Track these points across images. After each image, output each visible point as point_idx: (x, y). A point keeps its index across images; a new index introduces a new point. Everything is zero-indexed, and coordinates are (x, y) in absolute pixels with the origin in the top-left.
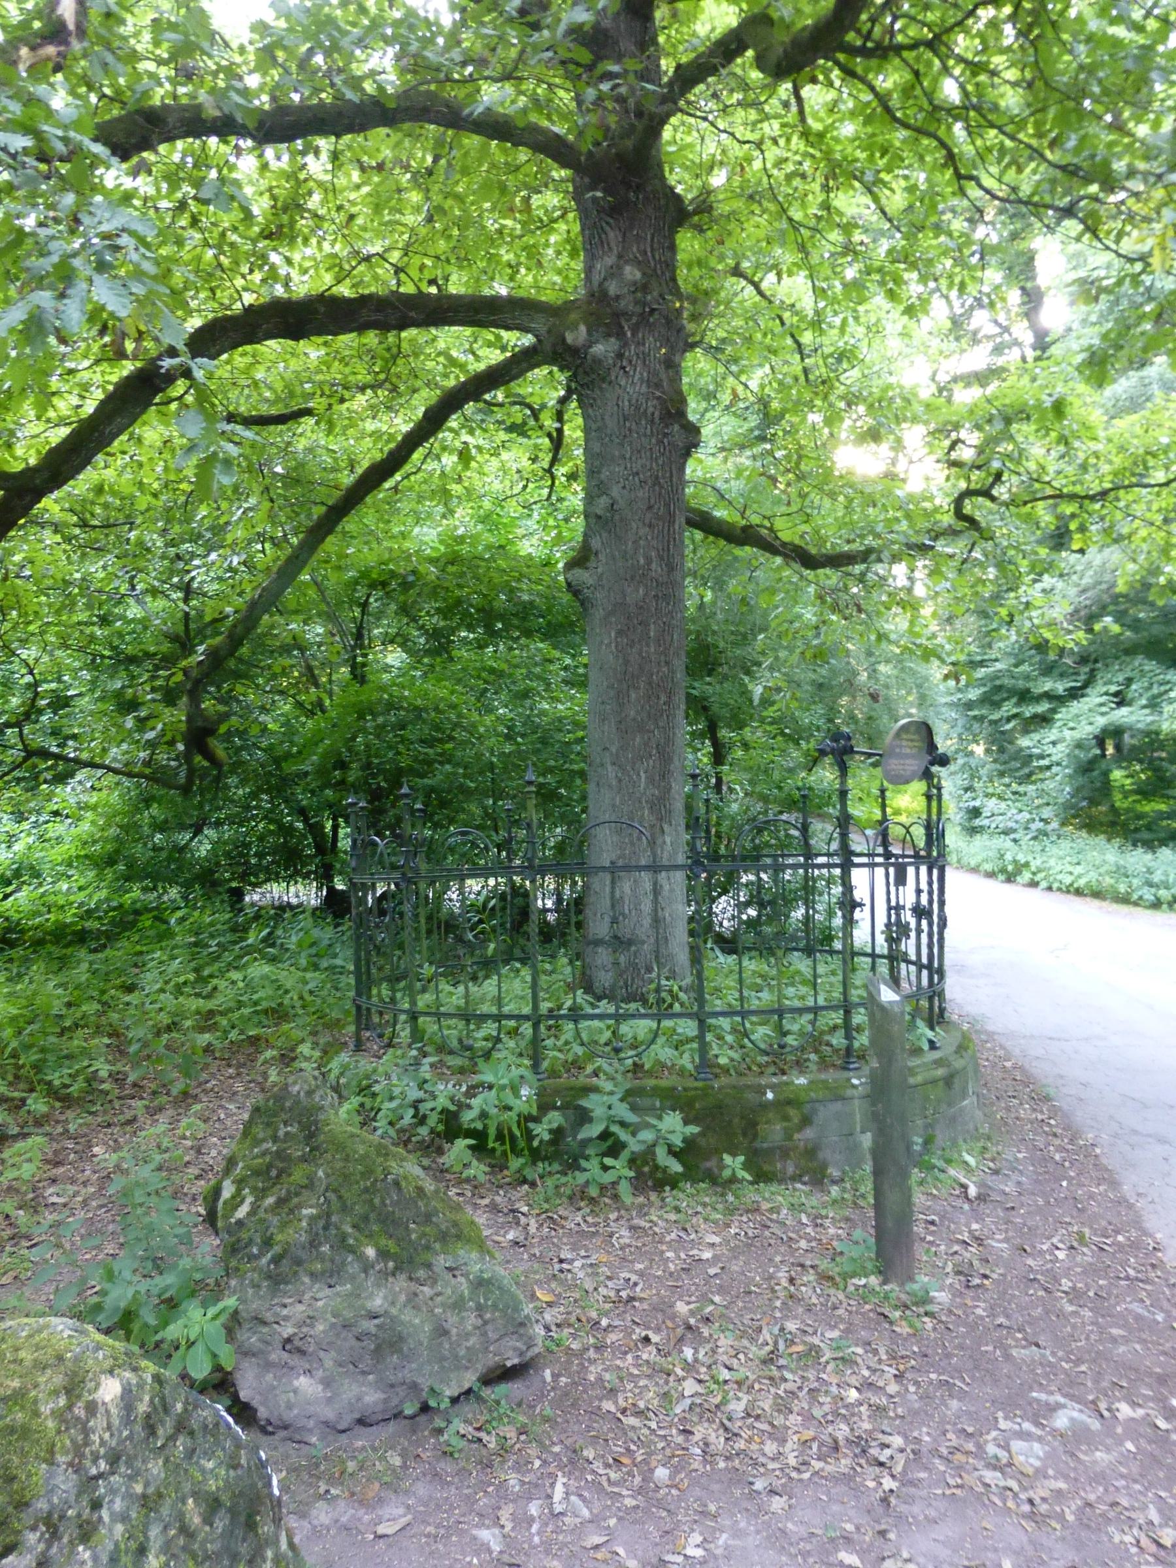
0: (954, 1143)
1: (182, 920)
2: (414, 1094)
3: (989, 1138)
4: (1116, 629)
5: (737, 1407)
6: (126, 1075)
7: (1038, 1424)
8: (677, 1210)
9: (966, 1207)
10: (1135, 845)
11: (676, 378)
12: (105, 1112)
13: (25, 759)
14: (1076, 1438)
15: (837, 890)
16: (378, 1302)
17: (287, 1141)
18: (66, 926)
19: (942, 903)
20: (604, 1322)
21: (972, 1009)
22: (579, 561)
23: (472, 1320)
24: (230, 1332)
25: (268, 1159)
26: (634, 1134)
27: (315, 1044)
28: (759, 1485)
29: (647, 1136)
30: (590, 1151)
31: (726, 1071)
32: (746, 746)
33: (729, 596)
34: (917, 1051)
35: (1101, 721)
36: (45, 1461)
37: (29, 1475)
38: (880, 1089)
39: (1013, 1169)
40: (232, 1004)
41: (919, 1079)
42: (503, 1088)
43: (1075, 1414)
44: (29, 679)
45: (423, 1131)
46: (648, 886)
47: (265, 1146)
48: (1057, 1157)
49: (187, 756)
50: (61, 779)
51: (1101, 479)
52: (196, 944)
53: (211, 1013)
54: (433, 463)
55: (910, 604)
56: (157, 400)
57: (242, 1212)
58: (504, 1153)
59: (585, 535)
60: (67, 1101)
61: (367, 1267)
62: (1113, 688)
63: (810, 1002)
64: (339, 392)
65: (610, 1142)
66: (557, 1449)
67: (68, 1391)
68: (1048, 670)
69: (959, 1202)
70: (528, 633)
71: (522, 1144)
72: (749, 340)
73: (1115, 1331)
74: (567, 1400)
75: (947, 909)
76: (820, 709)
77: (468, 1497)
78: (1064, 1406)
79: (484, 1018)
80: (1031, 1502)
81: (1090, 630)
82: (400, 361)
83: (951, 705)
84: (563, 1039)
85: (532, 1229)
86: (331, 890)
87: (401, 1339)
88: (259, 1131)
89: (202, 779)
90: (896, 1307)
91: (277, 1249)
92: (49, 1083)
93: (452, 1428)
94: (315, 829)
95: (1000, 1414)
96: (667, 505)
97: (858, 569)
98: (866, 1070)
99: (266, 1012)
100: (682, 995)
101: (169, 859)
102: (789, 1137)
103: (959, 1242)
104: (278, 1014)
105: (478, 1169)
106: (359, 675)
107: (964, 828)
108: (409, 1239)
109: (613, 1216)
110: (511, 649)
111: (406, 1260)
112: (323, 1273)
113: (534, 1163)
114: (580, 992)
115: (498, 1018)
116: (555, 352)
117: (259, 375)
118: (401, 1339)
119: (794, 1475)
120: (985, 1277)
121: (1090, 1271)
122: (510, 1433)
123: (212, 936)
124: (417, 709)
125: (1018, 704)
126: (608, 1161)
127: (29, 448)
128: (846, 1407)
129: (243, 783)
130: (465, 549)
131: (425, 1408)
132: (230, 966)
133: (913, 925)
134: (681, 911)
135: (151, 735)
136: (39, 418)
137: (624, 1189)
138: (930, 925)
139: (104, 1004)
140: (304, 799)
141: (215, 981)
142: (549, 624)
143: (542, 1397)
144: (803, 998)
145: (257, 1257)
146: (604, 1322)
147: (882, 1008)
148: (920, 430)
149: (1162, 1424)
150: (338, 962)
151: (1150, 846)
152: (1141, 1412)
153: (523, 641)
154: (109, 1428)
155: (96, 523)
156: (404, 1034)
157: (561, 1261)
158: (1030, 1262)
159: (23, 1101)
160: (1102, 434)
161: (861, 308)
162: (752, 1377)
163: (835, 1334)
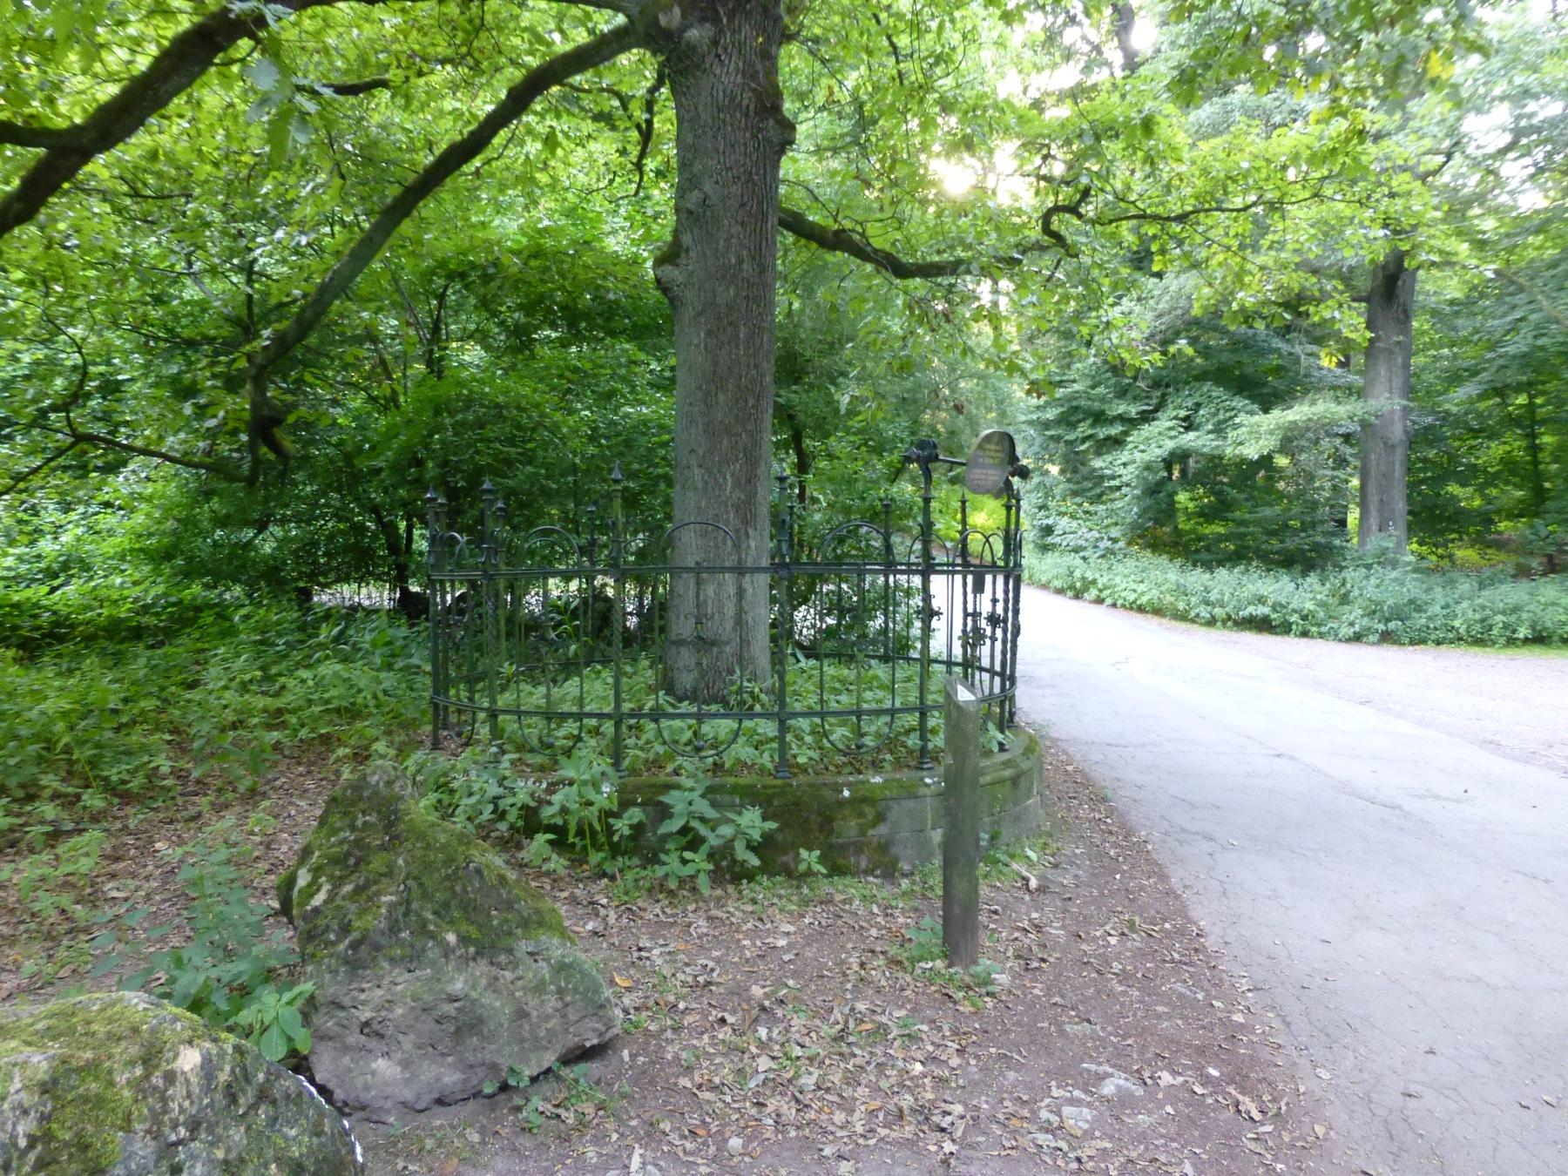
0: (1018, 840)
1: (247, 617)
2: (494, 790)
3: (1050, 835)
4: (1190, 351)
5: (809, 1081)
6: (189, 771)
7: (1087, 1092)
8: (754, 901)
9: (1027, 898)
10: (1195, 565)
11: (773, 70)
12: (167, 809)
13: (73, 445)
14: (1123, 1102)
15: (917, 601)
16: (459, 985)
17: (366, 831)
18: (122, 620)
19: (1016, 612)
20: (682, 1005)
21: (1038, 718)
22: (669, 257)
23: (552, 1002)
24: (306, 1017)
25: (346, 847)
26: (713, 830)
27: (390, 744)
28: (828, 1151)
29: (726, 830)
30: (670, 846)
31: (803, 769)
32: (831, 456)
33: (817, 305)
34: (988, 753)
35: (1170, 445)
36: (121, 1128)
37: (105, 1143)
38: (956, 783)
39: (1072, 864)
40: (302, 703)
41: (988, 779)
42: (585, 783)
43: (1121, 1082)
44: (77, 359)
45: (503, 826)
46: (731, 589)
47: (342, 835)
48: (1112, 853)
49: (252, 447)
50: (111, 469)
51: (1183, 200)
52: (262, 642)
53: (280, 712)
54: (517, 147)
55: (994, 318)
56: (217, 61)
57: (319, 899)
58: (584, 848)
59: (676, 233)
60: (127, 798)
61: (447, 952)
62: (1183, 413)
63: (888, 704)
64: (418, 64)
65: (689, 837)
66: (634, 1123)
67: (145, 1062)
68: (1122, 393)
69: (1020, 894)
70: (612, 333)
71: (602, 839)
72: (845, 41)
73: (1159, 1009)
74: (644, 1078)
75: (1021, 617)
76: (904, 422)
77: (546, 1169)
78: (1112, 1075)
79: (564, 717)
80: (1079, 1160)
81: (1164, 353)
82: (484, 35)
83: (1030, 423)
84: (644, 738)
85: (612, 919)
86: (405, 591)
87: (481, 1021)
88: (336, 820)
89: (266, 475)
90: (960, 988)
91: (355, 935)
92: (106, 779)
93: (531, 1106)
94: (388, 529)
95: (1053, 1083)
96: (760, 203)
97: (945, 281)
98: (940, 770)
99: (338, 710)
100: (763, 696)
101: (232, 556)
102: (864, 834)
103: (1018, 929)
104: (352, 713)
105: (558, 863)
106: (436, 366)
107: (1036, 545)
108: (491, 933)
109: (691, 907)
110: (595, 350)
111: (487, 946)
112: (402, 959)
113: (614, 858)
114: (661, 693)
115: (579, 717)
116: (648, 35)
117: (331, 41)
118: (481, 1021)
119: (861, 1141)
120: (1043, 960)
121: (1140, 955)
122: (589, 1109)
123: (279, 635)
124: (497, 406)
125: (1093, 426)
126: (688, 855)
127: (73, 105)
128: (912, 1079)
129: (312, 478)
130: (548, 243)
131: (504, 1087)
132: (298, 665)
133: (989, 633)
134: (763, 614)
135: (212, 423)
136: (84, 72)
137: (703, 882)
138: (1005, 631)
139: (165, 700)
140: (377, 497)
141: (283, 679)
142: (635, 325)
143: (619, 1076)
144: (880, 701)
145: (333, 944)
146: (682, 1005)
147: (958, 706)
148: (1013, 145)
149: (1199, 1090)
150: (415, 661)
151: (1209, 566)
152: (1180, 1079)
153: (608, 341)
154: (189, 1095)
155: (149, 193)
156: (484, 731)
157: (640, 949)
158: (1084, 947)
159: (78, 797)
160: (1186, 156)
161: (957, 14)
162: (823, 1053)
163: (902, 1013)
